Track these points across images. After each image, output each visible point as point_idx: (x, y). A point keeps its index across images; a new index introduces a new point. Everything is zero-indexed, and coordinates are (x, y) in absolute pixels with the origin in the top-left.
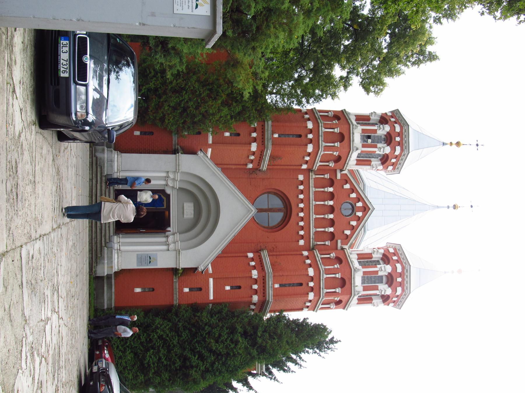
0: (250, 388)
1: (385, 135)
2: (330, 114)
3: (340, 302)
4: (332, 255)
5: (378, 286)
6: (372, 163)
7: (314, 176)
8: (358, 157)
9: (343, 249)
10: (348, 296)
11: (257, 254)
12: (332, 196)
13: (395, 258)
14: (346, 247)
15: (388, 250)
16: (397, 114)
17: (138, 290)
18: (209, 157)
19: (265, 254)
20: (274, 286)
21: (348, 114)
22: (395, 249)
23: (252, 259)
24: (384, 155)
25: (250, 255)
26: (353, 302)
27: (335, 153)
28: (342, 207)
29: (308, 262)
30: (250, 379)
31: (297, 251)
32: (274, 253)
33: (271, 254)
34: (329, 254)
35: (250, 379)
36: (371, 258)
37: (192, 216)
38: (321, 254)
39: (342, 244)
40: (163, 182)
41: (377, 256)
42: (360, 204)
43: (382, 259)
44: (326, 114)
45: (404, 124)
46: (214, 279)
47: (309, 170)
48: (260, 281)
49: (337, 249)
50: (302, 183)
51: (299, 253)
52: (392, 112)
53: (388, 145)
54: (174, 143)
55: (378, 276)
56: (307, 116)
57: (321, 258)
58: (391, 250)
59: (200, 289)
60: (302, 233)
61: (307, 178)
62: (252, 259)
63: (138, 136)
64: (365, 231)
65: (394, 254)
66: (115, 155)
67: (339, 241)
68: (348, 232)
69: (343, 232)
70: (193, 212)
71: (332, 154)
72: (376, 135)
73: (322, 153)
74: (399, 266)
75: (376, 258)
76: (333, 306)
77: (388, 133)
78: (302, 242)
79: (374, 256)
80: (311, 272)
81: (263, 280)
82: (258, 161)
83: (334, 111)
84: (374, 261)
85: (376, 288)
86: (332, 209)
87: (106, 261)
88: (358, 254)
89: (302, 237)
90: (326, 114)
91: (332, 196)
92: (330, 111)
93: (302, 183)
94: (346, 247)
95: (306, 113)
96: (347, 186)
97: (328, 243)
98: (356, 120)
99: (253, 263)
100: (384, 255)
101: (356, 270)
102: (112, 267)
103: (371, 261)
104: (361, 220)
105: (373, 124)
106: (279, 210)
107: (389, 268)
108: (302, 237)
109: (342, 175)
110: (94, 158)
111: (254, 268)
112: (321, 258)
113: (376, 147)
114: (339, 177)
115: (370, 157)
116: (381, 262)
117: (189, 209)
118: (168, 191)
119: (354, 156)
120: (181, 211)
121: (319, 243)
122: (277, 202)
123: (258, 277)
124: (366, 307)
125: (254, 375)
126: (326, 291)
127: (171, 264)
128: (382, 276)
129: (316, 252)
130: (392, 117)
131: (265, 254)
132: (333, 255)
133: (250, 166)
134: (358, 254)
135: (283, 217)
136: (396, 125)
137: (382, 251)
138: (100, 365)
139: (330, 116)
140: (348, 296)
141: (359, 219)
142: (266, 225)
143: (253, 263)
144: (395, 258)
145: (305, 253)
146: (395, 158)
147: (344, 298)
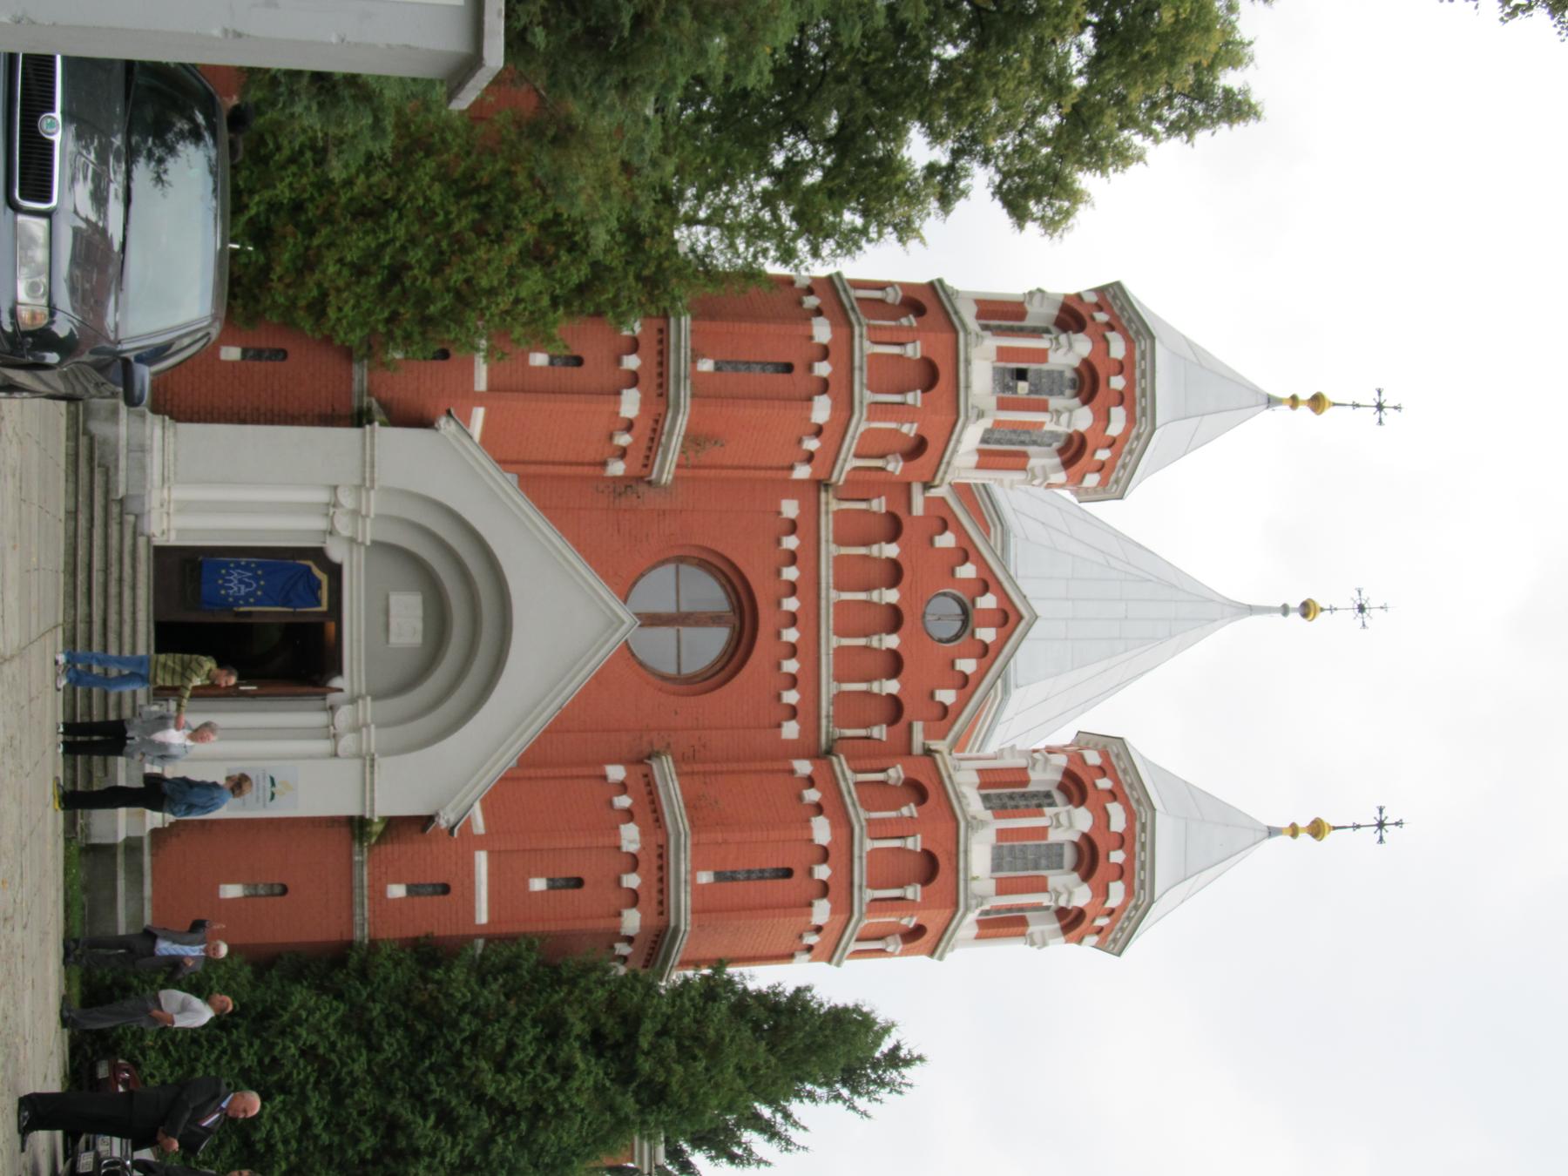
1: (1076, 370)
2: (892, 297)
3: (916, 933)
4: (892, 772)
5: (1044, 878)
6: (1033, 462)
7: (835, 505)
9: (929, 752)
10: (947, 913)
11: (640, 769)
12: (894, 573)
14: (935, 745)
16: (1115, 297)
19: (665, 771)
20: (694, 879)
21: (951, 294)
22: (1104, 754)
23: (623, 788)
25: (616, 773)
26: (960, 934)
27: (905, 428)
28: (930, 609)
29: (812, 795)
32: (697, 767)
34: (883, 770)
36: (1025, 783)
38: (856, 771)
39: (928, 734)
40: (320, 524)
42: (988, 602)
43: (1061, 787)
46: (491, 854)
47: (820, 484)
48: (649, 862)
49: (910, 753)
50: (793, 528)
52: (1101, 291)
53: (1085, 402)
56: (811, 302)
58: (1093, 758)
59: (445, 889)
61: (813, 511)
62: (623, 788)
63: (233, 363)
64: (1006, 691)
65: (1102, 771)
67: (918, 727)
68: (947, 696)
71: (896, 432)
72: (1045, 367)
73: (862, 428)
74: (1116, 812)
76: (894, 945)
77: (1086, 363)
78: (791, 730)
80: (822, 830)
81: (659, 859)
82: (644, 452)
83: (904, 286)
84: (1035, 795)
85: (1040, 886)
86: (894, 619)
88: (980, 772)
89: (793, 712)
91: (894, 573)
92: (891, 284)
93: (793, 528)
95: (810, 291)
96: (946, 540)
98: (979, 316)
99: (623, 801)
100: (1068, 774)
101: (974, 824)
103: (1023, 795)
104: (991, 654)
105: (1036, 332)
106: (714, 620)
107: (1083, 820)
108: (793, 712)
109: (928, 501)
110: (83, 441)
111: (629, 815)
113: (1043, 407)
114: (918, 507)
115: (1023, 443)
117: (408, 617)
118: (336, 553)
119: (970, 437)
120: (377, 622)
122: (708, 593)
123: (643, 848)
126: (870, 894)
127: (346, 805)
128: (1061, 845)
129: (840, 764)
130: (1099, 307)
132: (896, 774)
133: (617, 468)
134: (980, 772)
135: (728, 644)
136: (1111, 335)
137: (1061, 761)
139: (890, 299)
140: (947, 913)
142: (671, 669)
143: (623, 801)
144: (1104, 784)
145: (803, 767)
146: (1110, 446)
147: (933, 919)
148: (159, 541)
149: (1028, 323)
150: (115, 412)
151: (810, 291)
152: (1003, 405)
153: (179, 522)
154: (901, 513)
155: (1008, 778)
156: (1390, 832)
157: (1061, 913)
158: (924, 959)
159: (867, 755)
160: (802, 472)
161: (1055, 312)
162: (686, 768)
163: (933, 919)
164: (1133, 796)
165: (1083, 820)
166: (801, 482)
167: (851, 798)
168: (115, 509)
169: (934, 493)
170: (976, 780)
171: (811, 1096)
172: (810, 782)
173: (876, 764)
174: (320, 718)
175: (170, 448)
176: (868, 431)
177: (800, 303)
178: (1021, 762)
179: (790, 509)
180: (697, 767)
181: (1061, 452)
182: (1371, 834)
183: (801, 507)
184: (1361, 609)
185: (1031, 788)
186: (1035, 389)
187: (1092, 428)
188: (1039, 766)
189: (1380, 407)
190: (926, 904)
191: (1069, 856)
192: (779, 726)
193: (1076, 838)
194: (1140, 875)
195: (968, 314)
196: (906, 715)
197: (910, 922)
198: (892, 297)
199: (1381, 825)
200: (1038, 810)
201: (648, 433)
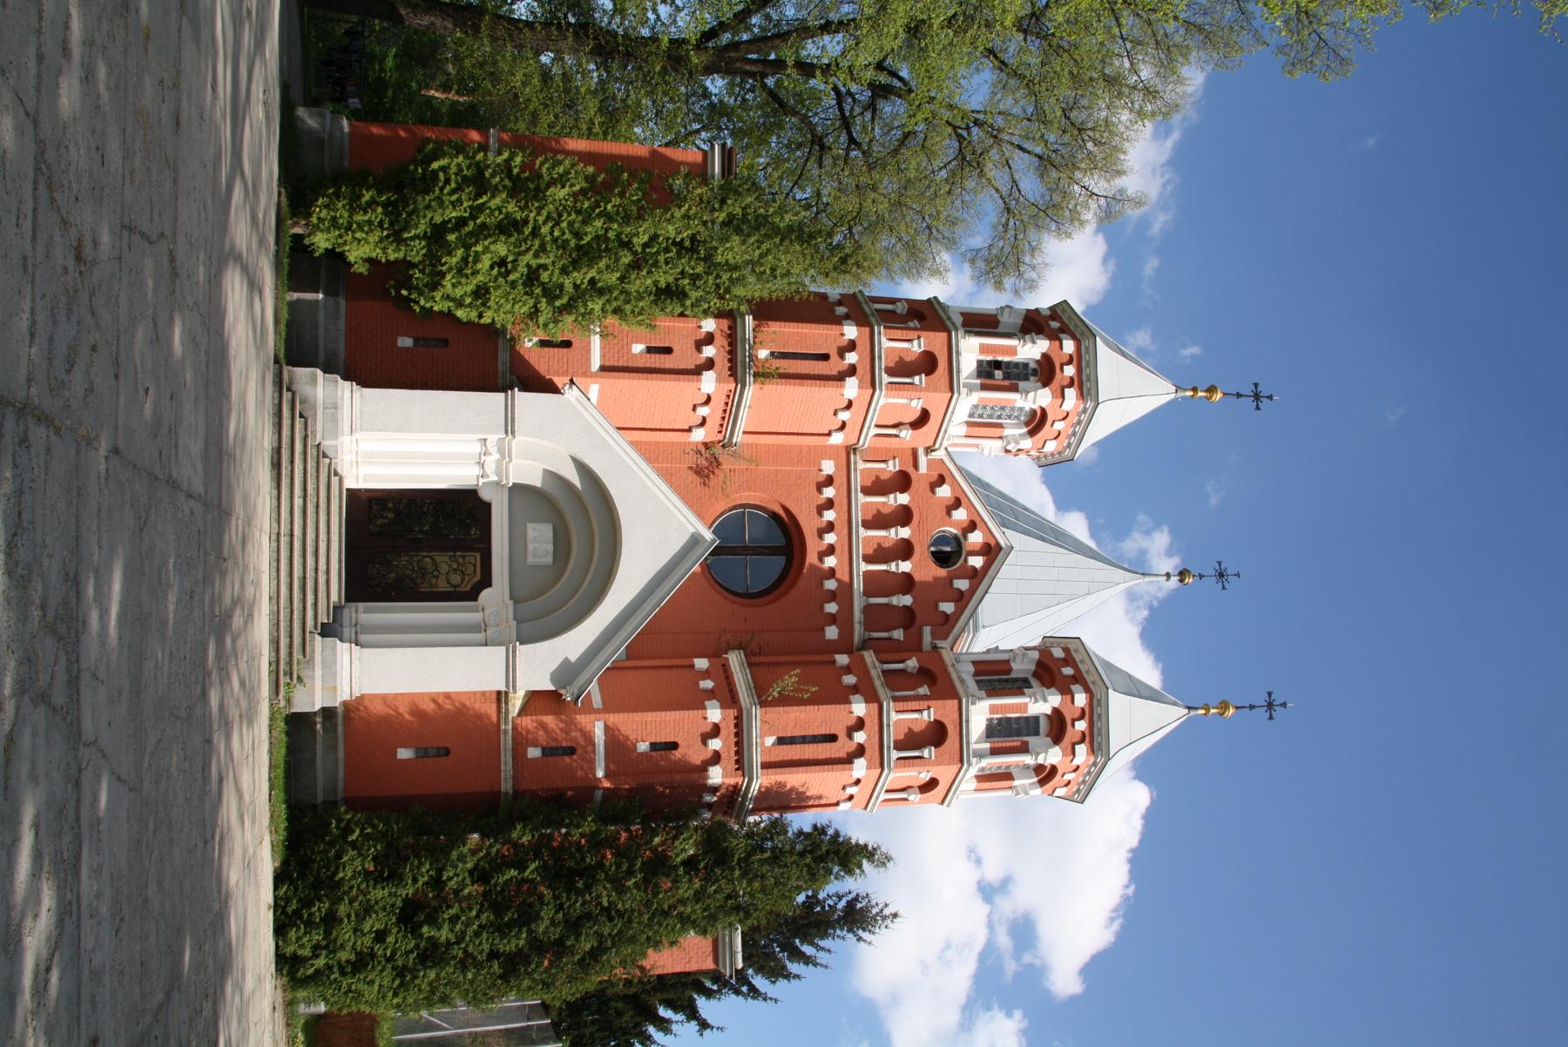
0: (704, 1025)
1: (1038, 362)
2: (901, 308)
3: (931, 784)
7: (861, 465)
8: (971, 415)
9: (935, 648)
10: (955, 768)
11: (718, 662)
13: (1068, 671)
14: (940, 643)
15: (1051, 655)
16: (1063, 311)
17: (405, 342)
18: (594, 399)
19: (735, 660)
21: (944, 307)
22: (1066, 650)
23: (706, 674)
24: (1034, 412)
25: (701, 663)
26: (964, 786)
30: (701, 1003)
31: (822, 653)
32: (762, 659)
33: (754, 659)
35: (701, 1003)
36: (1009, 671)
37: (549, 559)
38: (882, 662)
39: (934, 636)
41: (1021, 668)
43: (1036, 674)
44: (890, 307)
45: (1082, 334)
47: (851, 450)
51: (825, 658)
52: (1052, 309)
53: (1045, 385)
54: (500, 368)
55: (1027, 718)
56: (841, 310)
57: (885, 672)
58: (1058, 653)
59: (571, 751)
60: (832, 608)
62: (706, 674)
63: (407, 349)
64: (976, 629)
66: (346, 391)
67: (927, 630)
68: (948, 607)
69: (936, 606)
70: (550, 547)
73: (882, 402)
75: (1021, 671)
76: (914, 797)
78: (832, 633)
79: (1014, 666)
82: (719, 421)
83: (909, 301)
84: (1017, 680)
85: (1024, 749)
87: (318, 673)
88: (974, 663)
89: (833, 619)
90: (890, 307)
92: (900, 300)
94: (940, 643)
95: (840, 303)
97: (898, 634)
99: (707, 684)
100: (1040, 664)
102: (335, 689)
103: (1007, 681)
106: (774, 551)
108: (833, 619)
109: (930, 463)
110: (287, 396)
112: (885, 672)
113: (1015, 389)
116: (1034, 682)
117: (540, 538)
121: (876, 635)
124: (998, 796)
125: (709, 994)
128: (1036, 718)
129: (869, 657)
131: (735, 660)
132: (912, 664)
134: (974, 663)
137: (1035, 655)
138: (868, 204)
140: (955, 768)
141: (976, 576)
143: (707, 684)
144: (1068, 671)
145: (842, 659)
147: (944, 773)
148: (351, 483)
149: (999, 330)
150: (314, 380)
151: (840, 303)
152: (984, 388)
153: (365, 470)
154: (910, 470)
155: (992, 668)
156: (1278, 712)
157: (1039, 769)
158: (935, 807)
159: (886, 650)
160: (837, 439)
161: (1020, 322)
162: (754, 659)
163: (944, 773)
164: (1089, 679)
165: (1055, 700)
166: (836, 447)
167: (878, 683)
168: (311, 452)
169: (934, 455)
170: (972, 669)
171: (1127, 887)
172: (848, 670)
173: (897, 656)
174: (475, 617)
175: (357, 407)
176: (885, 405)
177: (833, 311)
178: (1005, 657)
179: (828, 467)
180: (762, 659)
181: (1027, 424)
182: (1262, 713)
183: (836, 466)
184: (1221, 575)
185: (1013, 675)
186: (1007, 377)
187: (1051, 404)
188: (1019, 659)
189: (1257, 397)
190: (938, 762)
191: (1044, 725)
192: (823, 630)
193: (1049, 712)
194: (1097, 739)
195: (958, 320)
196: (918, 621)
197: (925, 777)
198: (901, 308)
199: (1270, 706)
200: (1019, 692)
201: (722, 406)
